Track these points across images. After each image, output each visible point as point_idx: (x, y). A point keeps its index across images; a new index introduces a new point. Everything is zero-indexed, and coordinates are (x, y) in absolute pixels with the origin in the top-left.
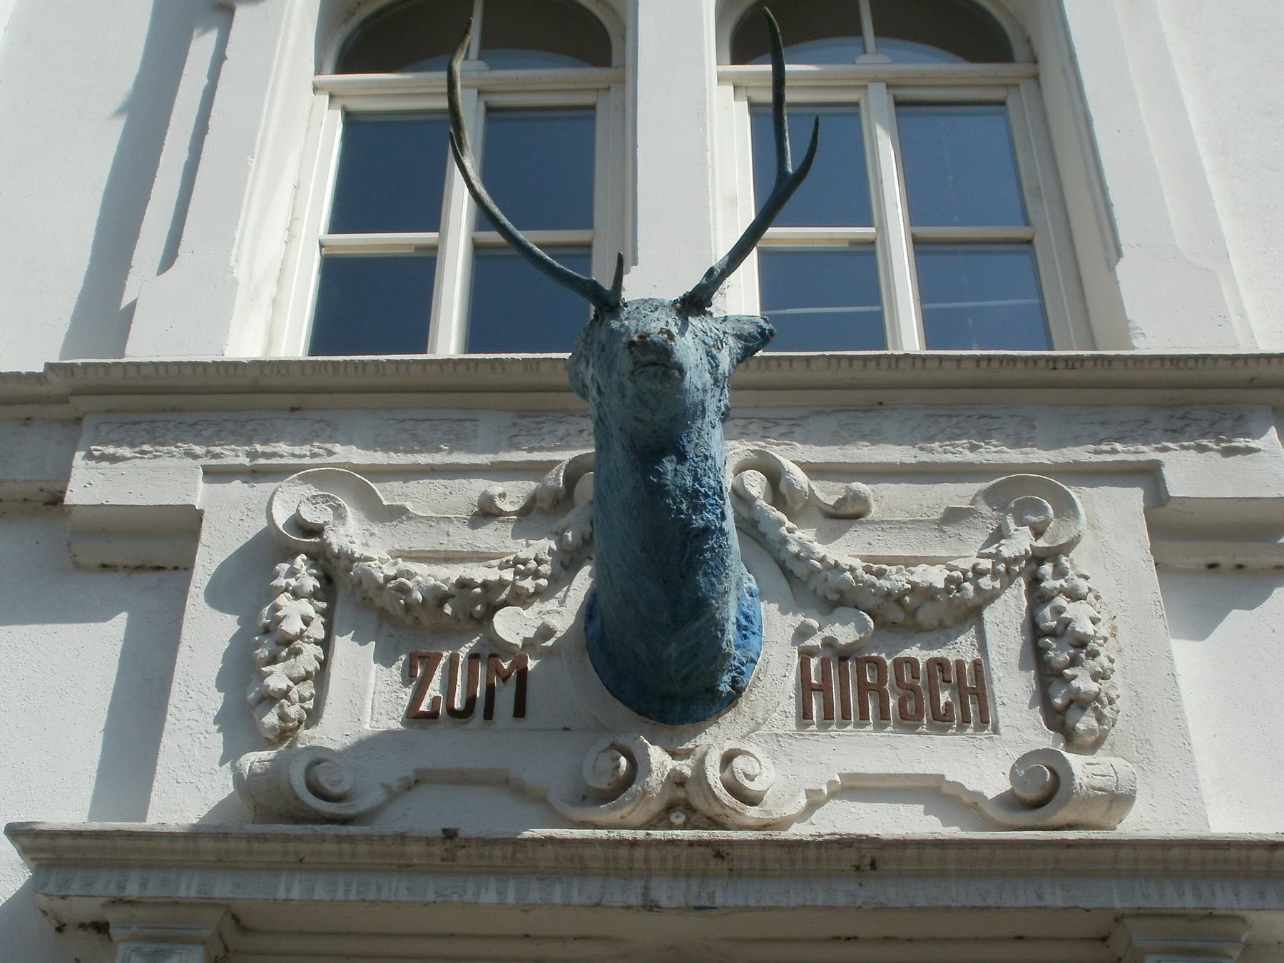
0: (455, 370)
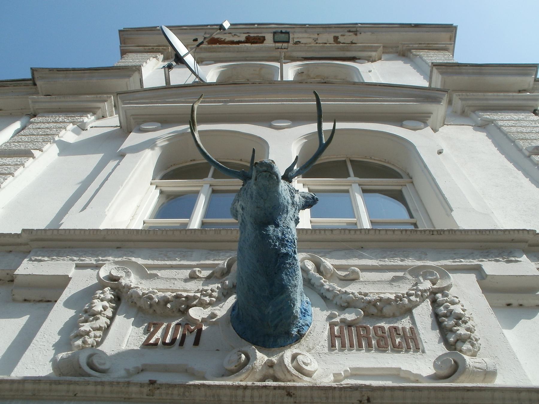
0: (186, 233)
